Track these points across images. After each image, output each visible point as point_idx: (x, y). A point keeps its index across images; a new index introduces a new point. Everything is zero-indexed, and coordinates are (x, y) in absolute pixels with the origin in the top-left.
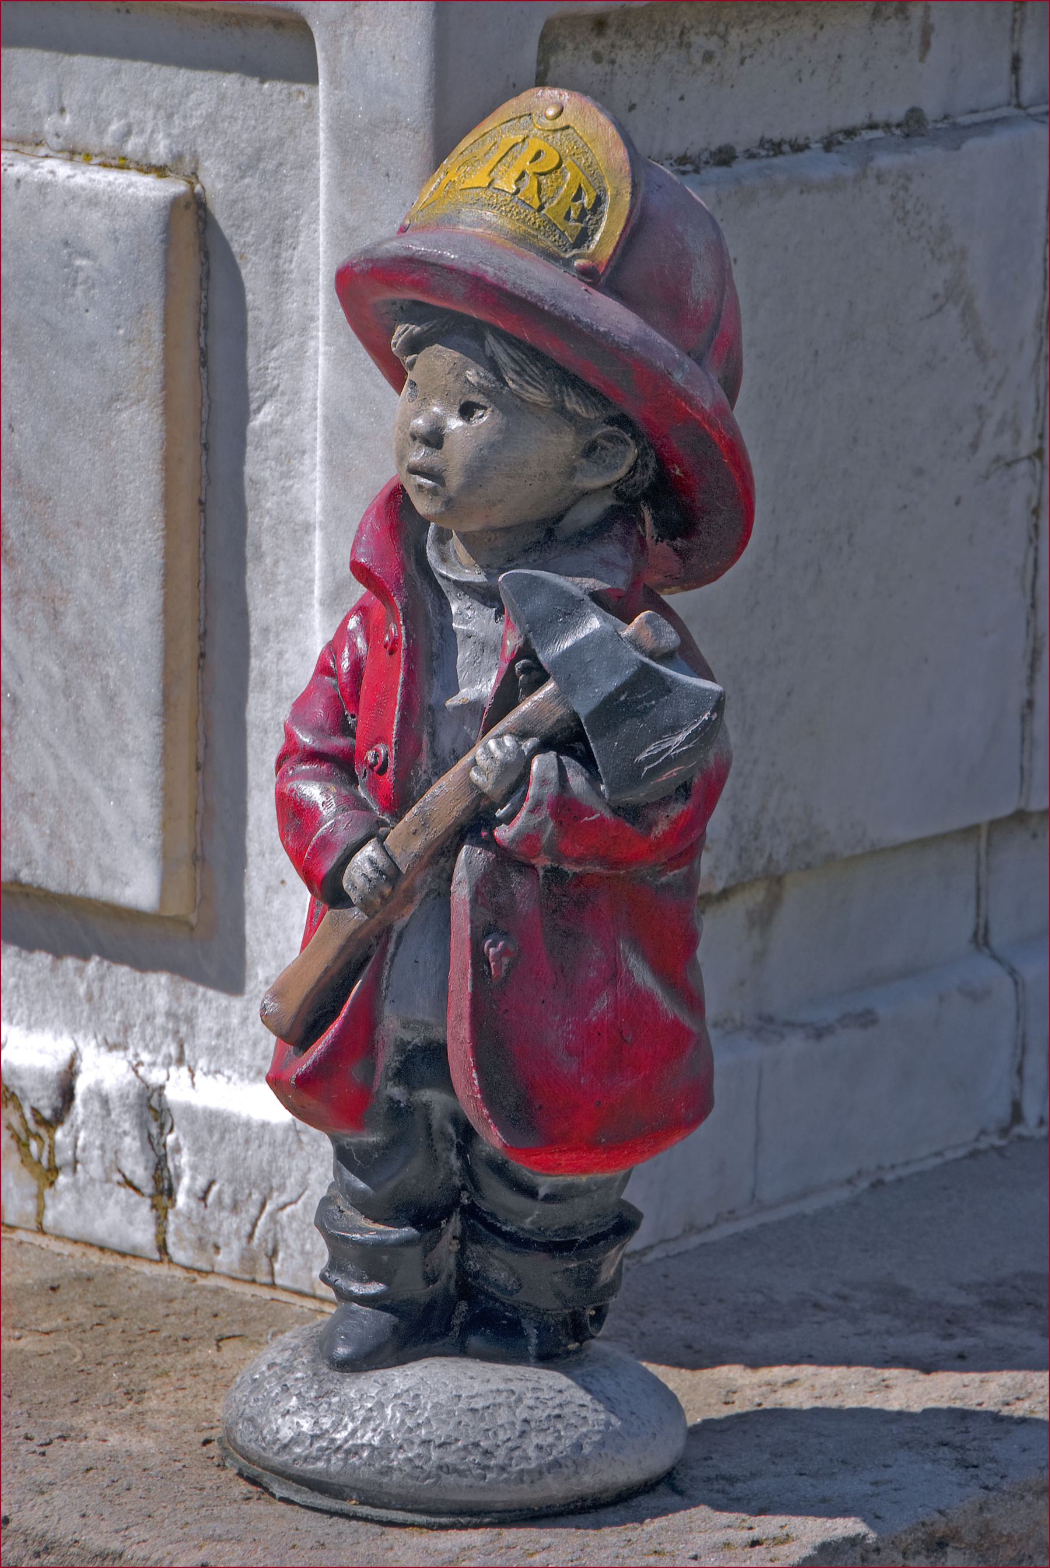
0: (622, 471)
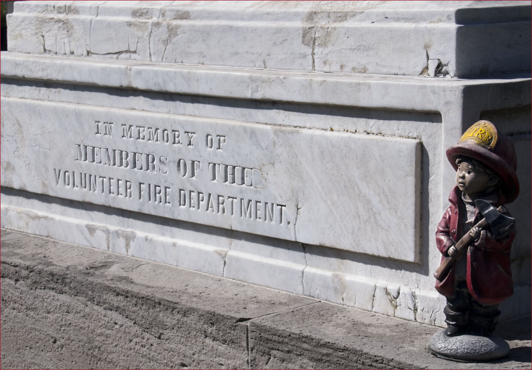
0: (496, 183)
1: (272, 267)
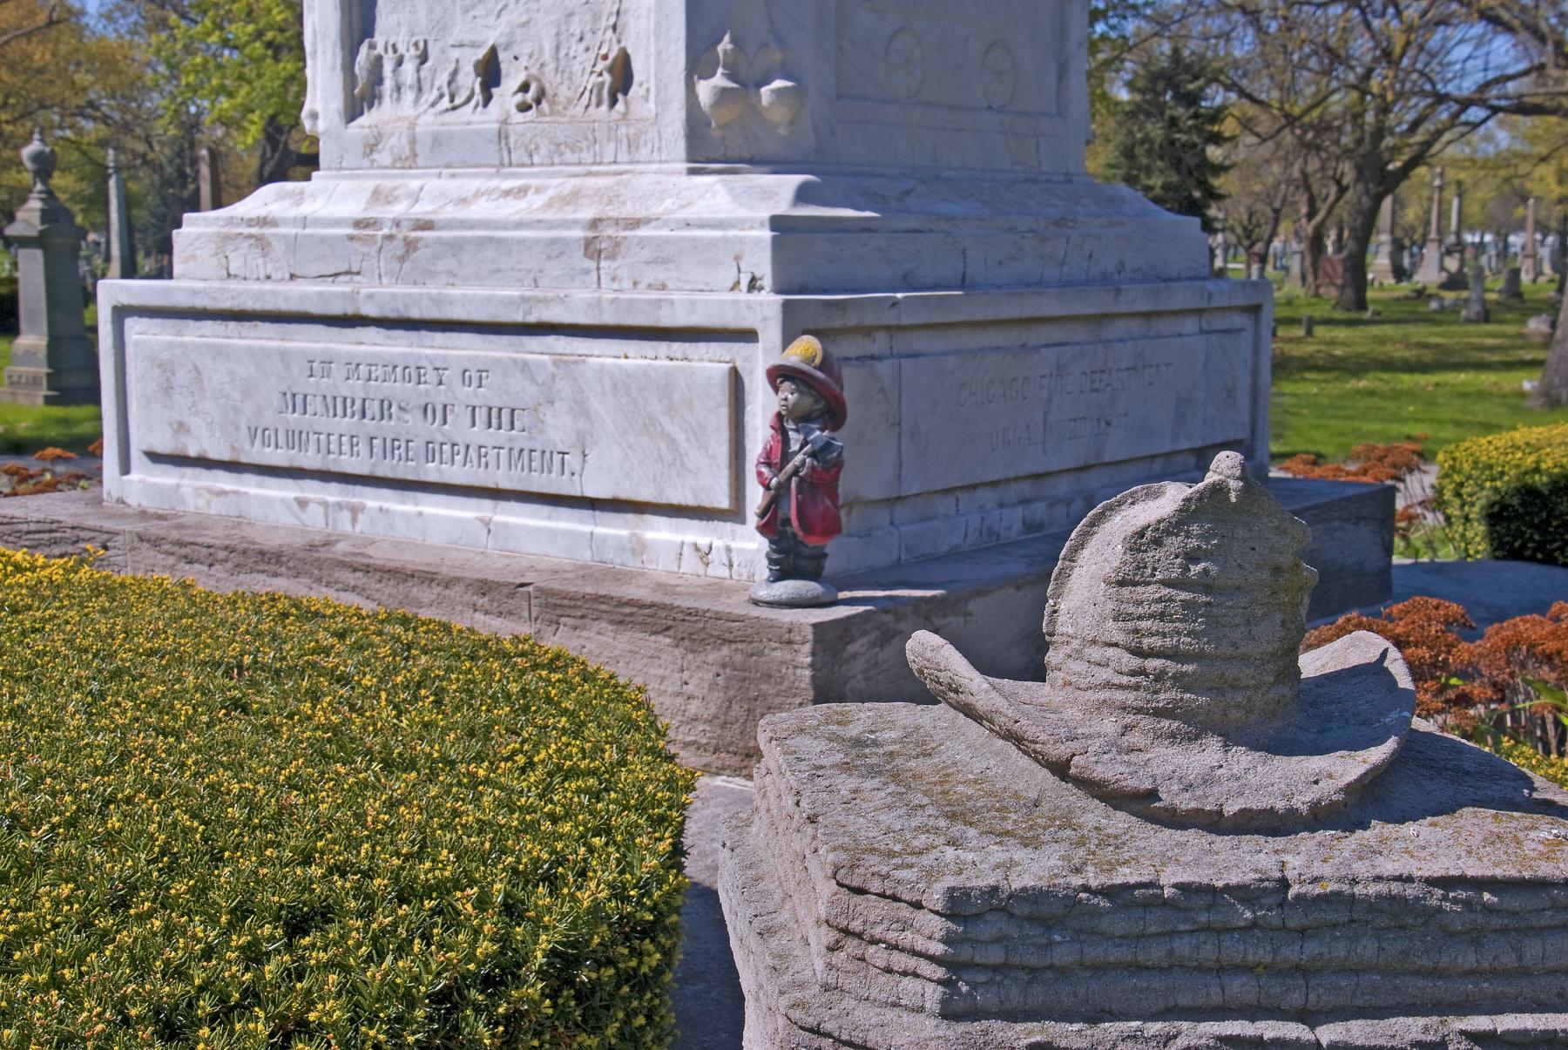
1: (553, 533)
